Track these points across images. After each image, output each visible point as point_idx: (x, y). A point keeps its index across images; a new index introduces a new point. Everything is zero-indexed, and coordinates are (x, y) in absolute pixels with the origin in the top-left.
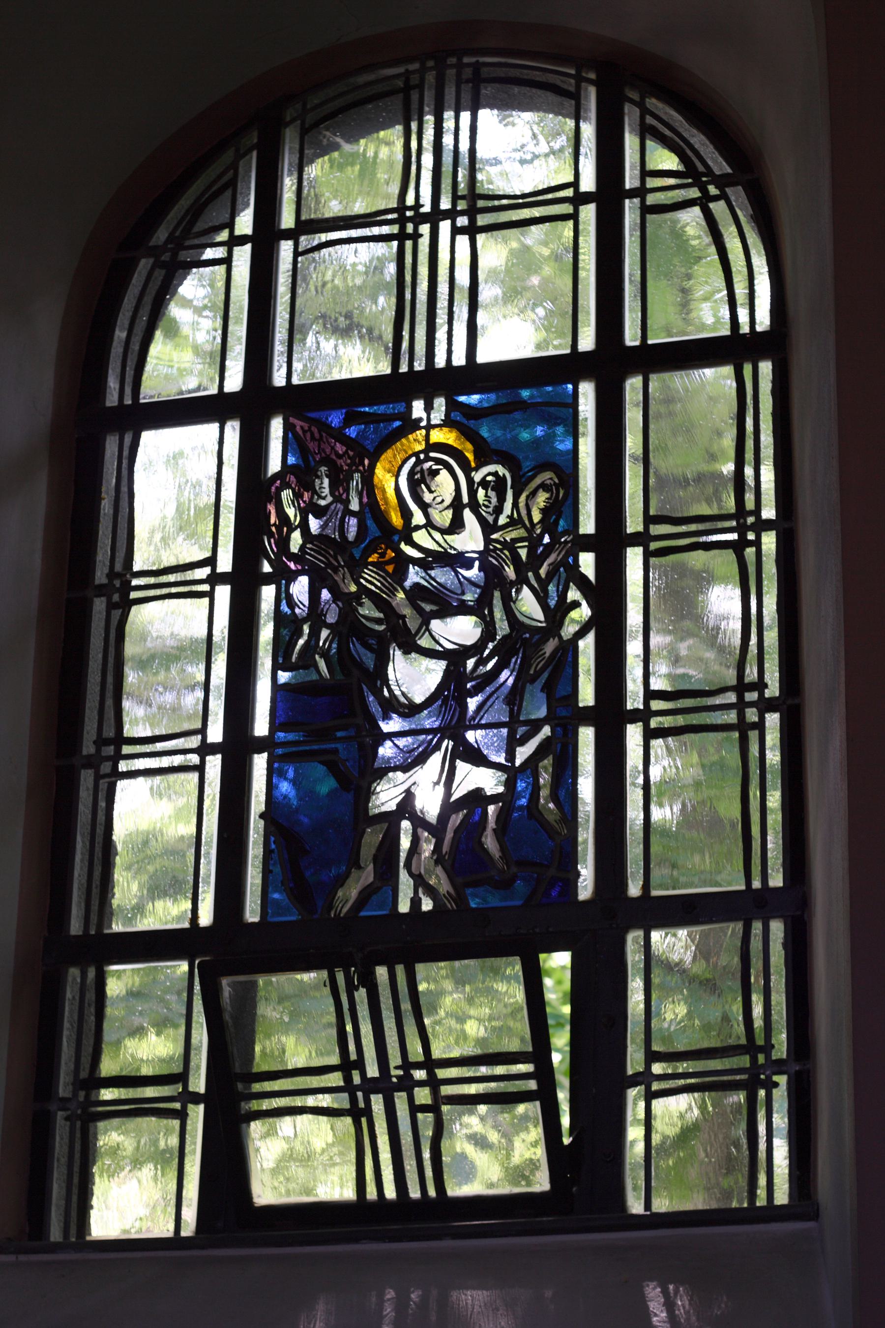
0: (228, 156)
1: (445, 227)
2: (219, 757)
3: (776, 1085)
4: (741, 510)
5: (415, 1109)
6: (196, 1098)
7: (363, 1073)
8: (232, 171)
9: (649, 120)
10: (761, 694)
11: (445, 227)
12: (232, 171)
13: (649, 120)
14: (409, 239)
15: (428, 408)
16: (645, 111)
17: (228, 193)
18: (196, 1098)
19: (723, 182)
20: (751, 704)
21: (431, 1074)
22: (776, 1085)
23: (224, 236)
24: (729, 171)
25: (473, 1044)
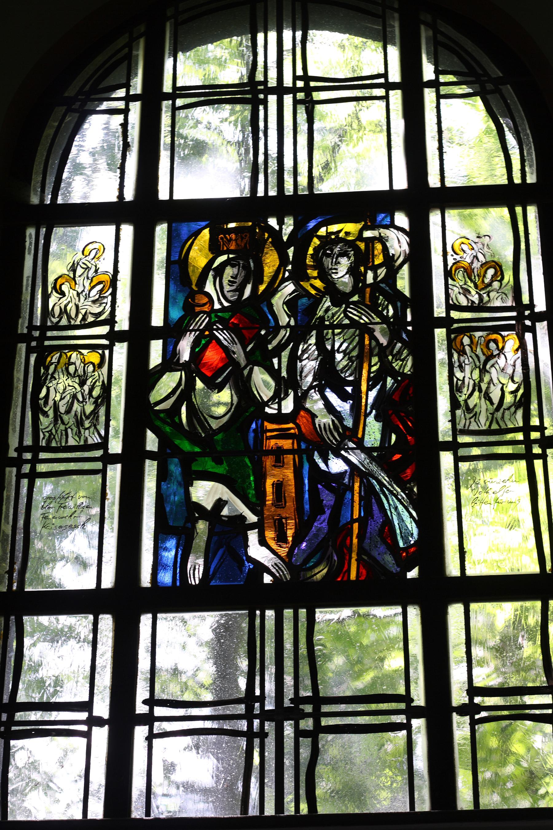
0: (123, 40)
1: (288, 99)
2: (119, 466)
3: (145, 702)
4: (519, 306)
5: (299, 733)
6: (99, 722)
7: (262, 706)
8: (127, 49)
9: (440, 37)
10: (543, 434)
11: (288, 99)
12: (127, 49)
13: (440, 37)
14: (309, 84)
15: (281, 223)
16: (436, 32)
17: (125, 65)
18: (99, 722)
19: (497, 82)
20: (535, 441)
21: (317, 709)
22: (145, 702)
23: (121, 93)
24: (501, 75)
25: (45, 679)
